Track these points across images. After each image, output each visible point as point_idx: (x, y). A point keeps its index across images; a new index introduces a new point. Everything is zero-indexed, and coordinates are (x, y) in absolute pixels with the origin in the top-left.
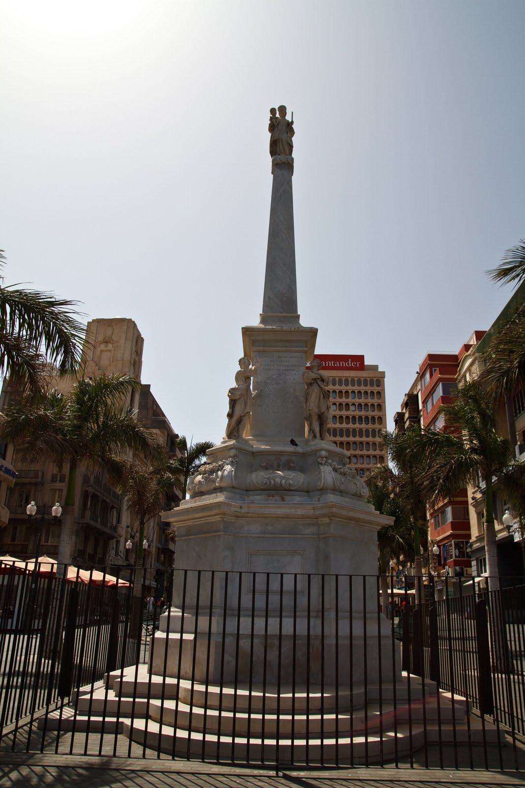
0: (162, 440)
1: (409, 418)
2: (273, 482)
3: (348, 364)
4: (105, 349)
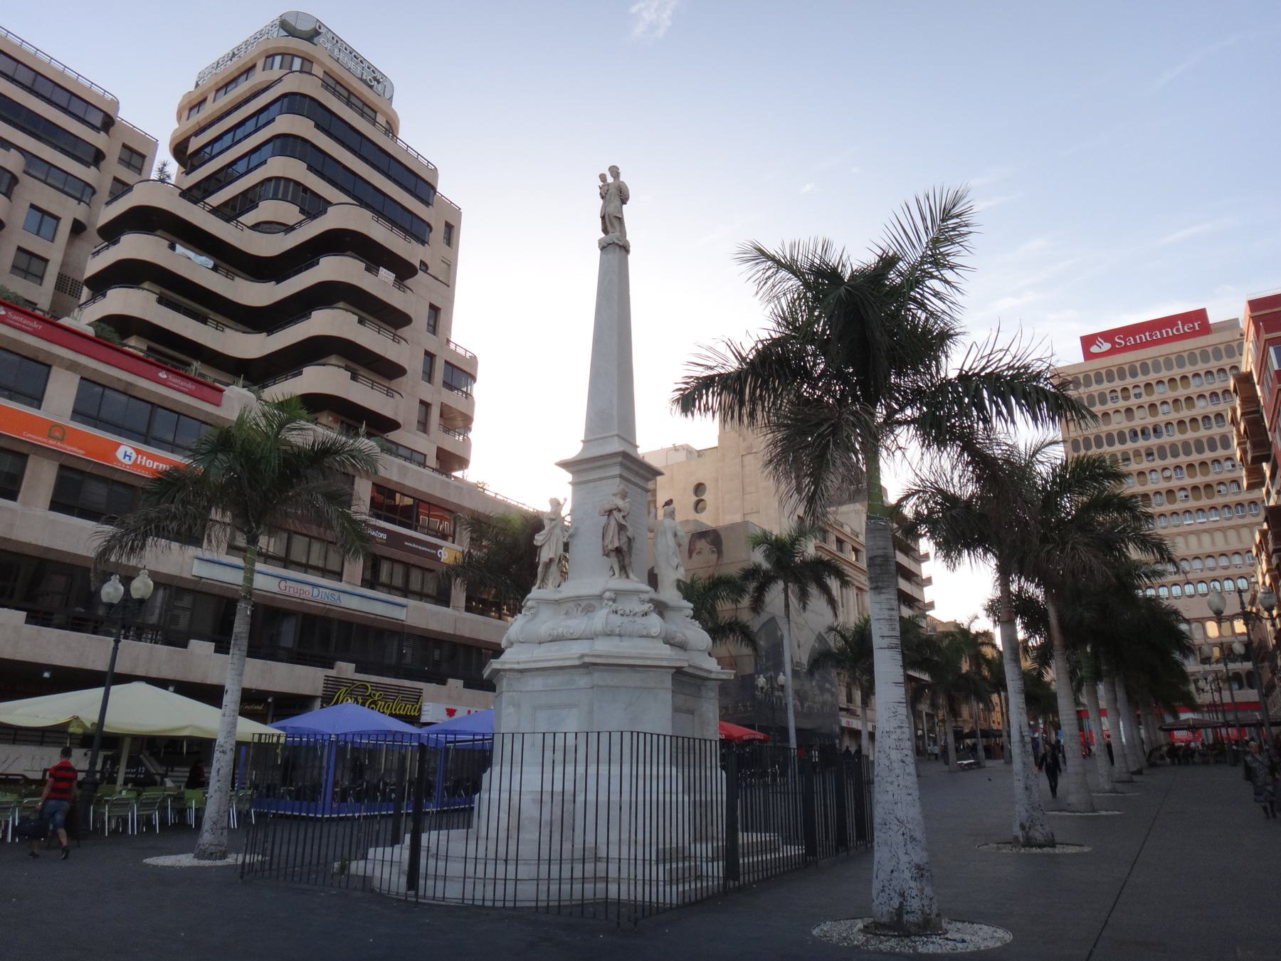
0: (161, 593)
1: (1242, 414)
3: (1178, 330)
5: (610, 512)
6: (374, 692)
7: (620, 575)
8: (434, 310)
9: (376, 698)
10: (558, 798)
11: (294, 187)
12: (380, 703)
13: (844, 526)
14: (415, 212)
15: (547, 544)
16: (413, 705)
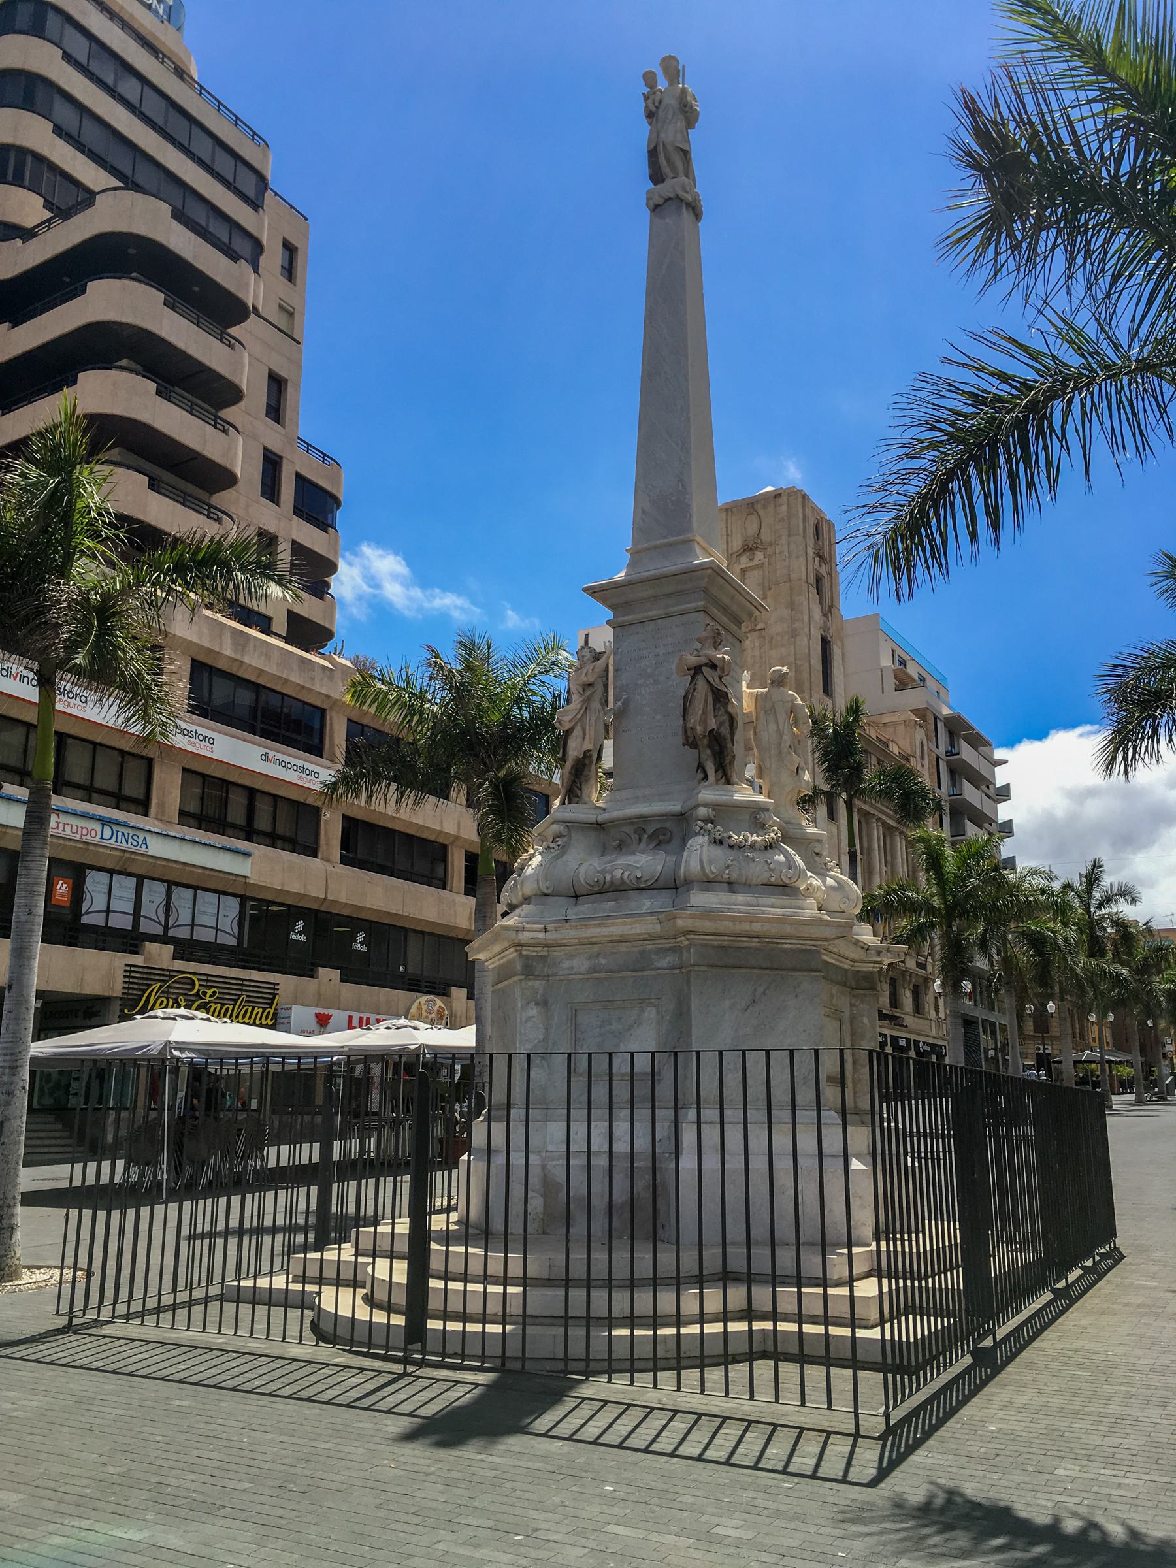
2: (608, 878)
4: (751, 564)
5: (697, 670)
6: (203, 989)
7: (717, 781)
8: (277, 383)
9: (208, 999)
10: (621, 1166)
11: (32, 162)
12: (213, 1006)
13: (890, 744)
14: (236, 218)
15: (578, 727)
16: (264, 1009)
